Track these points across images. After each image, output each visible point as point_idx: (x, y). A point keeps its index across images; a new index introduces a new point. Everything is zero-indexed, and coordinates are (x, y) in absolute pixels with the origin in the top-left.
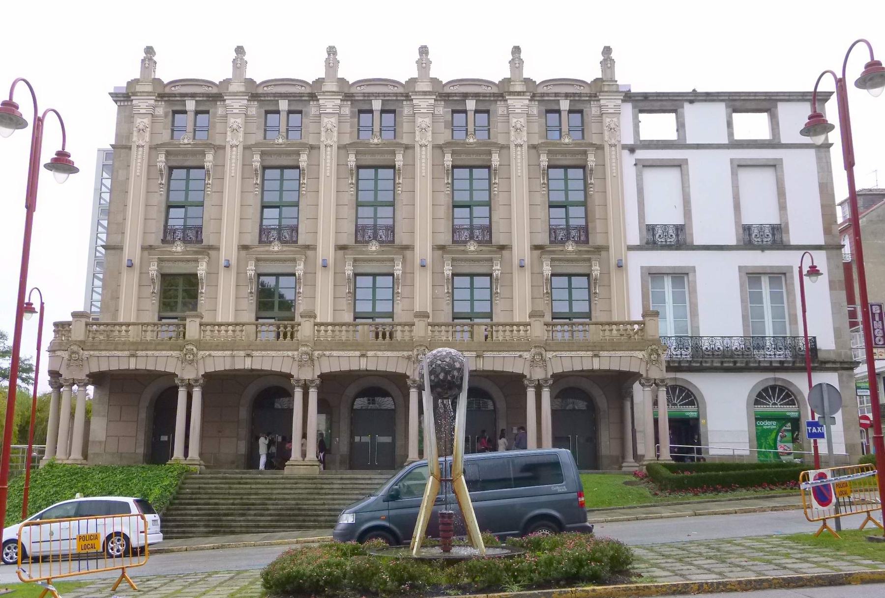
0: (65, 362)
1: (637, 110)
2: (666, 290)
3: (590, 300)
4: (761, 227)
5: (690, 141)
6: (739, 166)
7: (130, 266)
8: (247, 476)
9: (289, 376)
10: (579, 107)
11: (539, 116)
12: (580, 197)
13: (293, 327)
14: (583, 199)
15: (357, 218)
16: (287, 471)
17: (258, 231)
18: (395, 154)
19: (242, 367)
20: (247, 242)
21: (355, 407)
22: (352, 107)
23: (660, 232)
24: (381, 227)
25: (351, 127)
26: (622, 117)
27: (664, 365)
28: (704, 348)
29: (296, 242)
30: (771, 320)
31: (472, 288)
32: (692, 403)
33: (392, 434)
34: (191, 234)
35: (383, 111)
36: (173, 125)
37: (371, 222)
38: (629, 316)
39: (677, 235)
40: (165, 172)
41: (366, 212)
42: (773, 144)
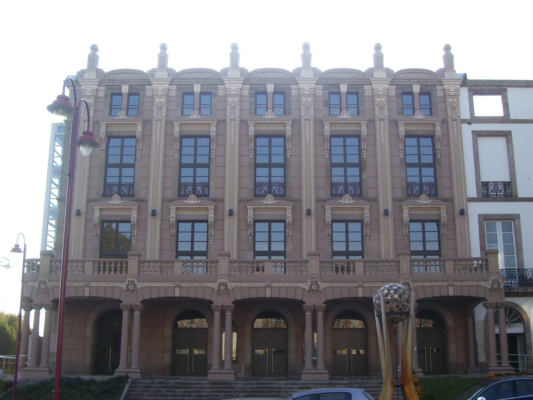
1: (472, 93)
2: (498, 232)
3: (362, 242)
4: (496, 183)
5: (512, 117)
11: (397, 97)
12: (280, 160)
14: (432, 162)
15: (255, 176)
16: (210, 377)
17: (177, 186)
19: (186, 296)
20: (94, 195)
21: (255, 327)
23: (492, 187)
26: (460, 98)
27: (503, 291)
28: (528, 278)
29: (208, 196)
31: (193, 232)
33: (206, 349)
36: (111, 104)
37: (116, 180)
38: (470, 255)
39: (505, 190)
42: (506, 119)
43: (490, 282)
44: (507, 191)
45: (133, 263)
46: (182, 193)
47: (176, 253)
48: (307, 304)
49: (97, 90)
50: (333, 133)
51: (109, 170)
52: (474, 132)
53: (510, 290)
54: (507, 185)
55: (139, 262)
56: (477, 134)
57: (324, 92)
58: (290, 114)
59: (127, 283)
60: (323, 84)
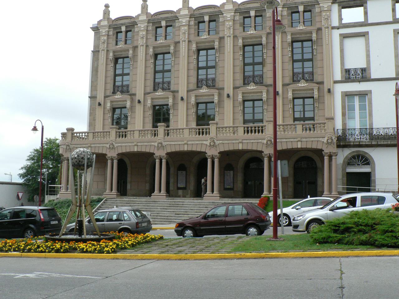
0: (65, 150)
1: (341, 7)
2: (356, 104)
4: (356, 70)
5: (370, 21)
6: (344, 37)
7: (228, 96)
8: (136, 200)
9: (261, 152)
10: (308, 8)
11: (288, 16)
13: (262, 127)
17: (152, 84)
18: (214, 42)
22: (195, 21)
23: (353, 72)
24: (257, 76)
25: (195, 30)
30: (359, 119)
31: (254, 107)
32: (368, 164)
34: (210, 82)
35: (304, 11)
39: (362, 74)
40: (196, 53)
41: (298, 65)
43: (326, 139)
44: (363, 75)
45: (212, 128)
46: (295, 79)
47: (294, 119)
48: (265, 153)
49: (108, 31)
50: (294, 39)
51: (200, 71)
52: (341, 35)
53: (359, 143)
54: (363, 70)
55: (217, 128)
56: (344, 37)
57: (240, 17)
58: (219, 34)
59: (109, 144)
60: (239, 12)
